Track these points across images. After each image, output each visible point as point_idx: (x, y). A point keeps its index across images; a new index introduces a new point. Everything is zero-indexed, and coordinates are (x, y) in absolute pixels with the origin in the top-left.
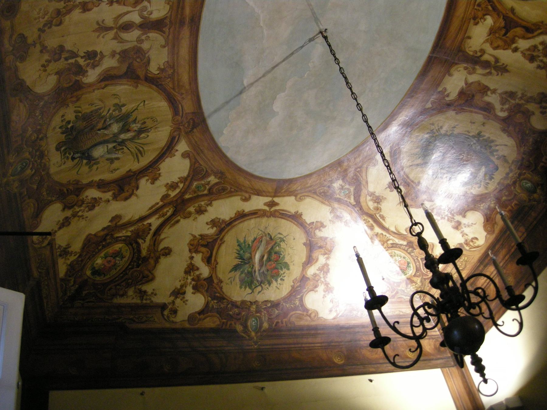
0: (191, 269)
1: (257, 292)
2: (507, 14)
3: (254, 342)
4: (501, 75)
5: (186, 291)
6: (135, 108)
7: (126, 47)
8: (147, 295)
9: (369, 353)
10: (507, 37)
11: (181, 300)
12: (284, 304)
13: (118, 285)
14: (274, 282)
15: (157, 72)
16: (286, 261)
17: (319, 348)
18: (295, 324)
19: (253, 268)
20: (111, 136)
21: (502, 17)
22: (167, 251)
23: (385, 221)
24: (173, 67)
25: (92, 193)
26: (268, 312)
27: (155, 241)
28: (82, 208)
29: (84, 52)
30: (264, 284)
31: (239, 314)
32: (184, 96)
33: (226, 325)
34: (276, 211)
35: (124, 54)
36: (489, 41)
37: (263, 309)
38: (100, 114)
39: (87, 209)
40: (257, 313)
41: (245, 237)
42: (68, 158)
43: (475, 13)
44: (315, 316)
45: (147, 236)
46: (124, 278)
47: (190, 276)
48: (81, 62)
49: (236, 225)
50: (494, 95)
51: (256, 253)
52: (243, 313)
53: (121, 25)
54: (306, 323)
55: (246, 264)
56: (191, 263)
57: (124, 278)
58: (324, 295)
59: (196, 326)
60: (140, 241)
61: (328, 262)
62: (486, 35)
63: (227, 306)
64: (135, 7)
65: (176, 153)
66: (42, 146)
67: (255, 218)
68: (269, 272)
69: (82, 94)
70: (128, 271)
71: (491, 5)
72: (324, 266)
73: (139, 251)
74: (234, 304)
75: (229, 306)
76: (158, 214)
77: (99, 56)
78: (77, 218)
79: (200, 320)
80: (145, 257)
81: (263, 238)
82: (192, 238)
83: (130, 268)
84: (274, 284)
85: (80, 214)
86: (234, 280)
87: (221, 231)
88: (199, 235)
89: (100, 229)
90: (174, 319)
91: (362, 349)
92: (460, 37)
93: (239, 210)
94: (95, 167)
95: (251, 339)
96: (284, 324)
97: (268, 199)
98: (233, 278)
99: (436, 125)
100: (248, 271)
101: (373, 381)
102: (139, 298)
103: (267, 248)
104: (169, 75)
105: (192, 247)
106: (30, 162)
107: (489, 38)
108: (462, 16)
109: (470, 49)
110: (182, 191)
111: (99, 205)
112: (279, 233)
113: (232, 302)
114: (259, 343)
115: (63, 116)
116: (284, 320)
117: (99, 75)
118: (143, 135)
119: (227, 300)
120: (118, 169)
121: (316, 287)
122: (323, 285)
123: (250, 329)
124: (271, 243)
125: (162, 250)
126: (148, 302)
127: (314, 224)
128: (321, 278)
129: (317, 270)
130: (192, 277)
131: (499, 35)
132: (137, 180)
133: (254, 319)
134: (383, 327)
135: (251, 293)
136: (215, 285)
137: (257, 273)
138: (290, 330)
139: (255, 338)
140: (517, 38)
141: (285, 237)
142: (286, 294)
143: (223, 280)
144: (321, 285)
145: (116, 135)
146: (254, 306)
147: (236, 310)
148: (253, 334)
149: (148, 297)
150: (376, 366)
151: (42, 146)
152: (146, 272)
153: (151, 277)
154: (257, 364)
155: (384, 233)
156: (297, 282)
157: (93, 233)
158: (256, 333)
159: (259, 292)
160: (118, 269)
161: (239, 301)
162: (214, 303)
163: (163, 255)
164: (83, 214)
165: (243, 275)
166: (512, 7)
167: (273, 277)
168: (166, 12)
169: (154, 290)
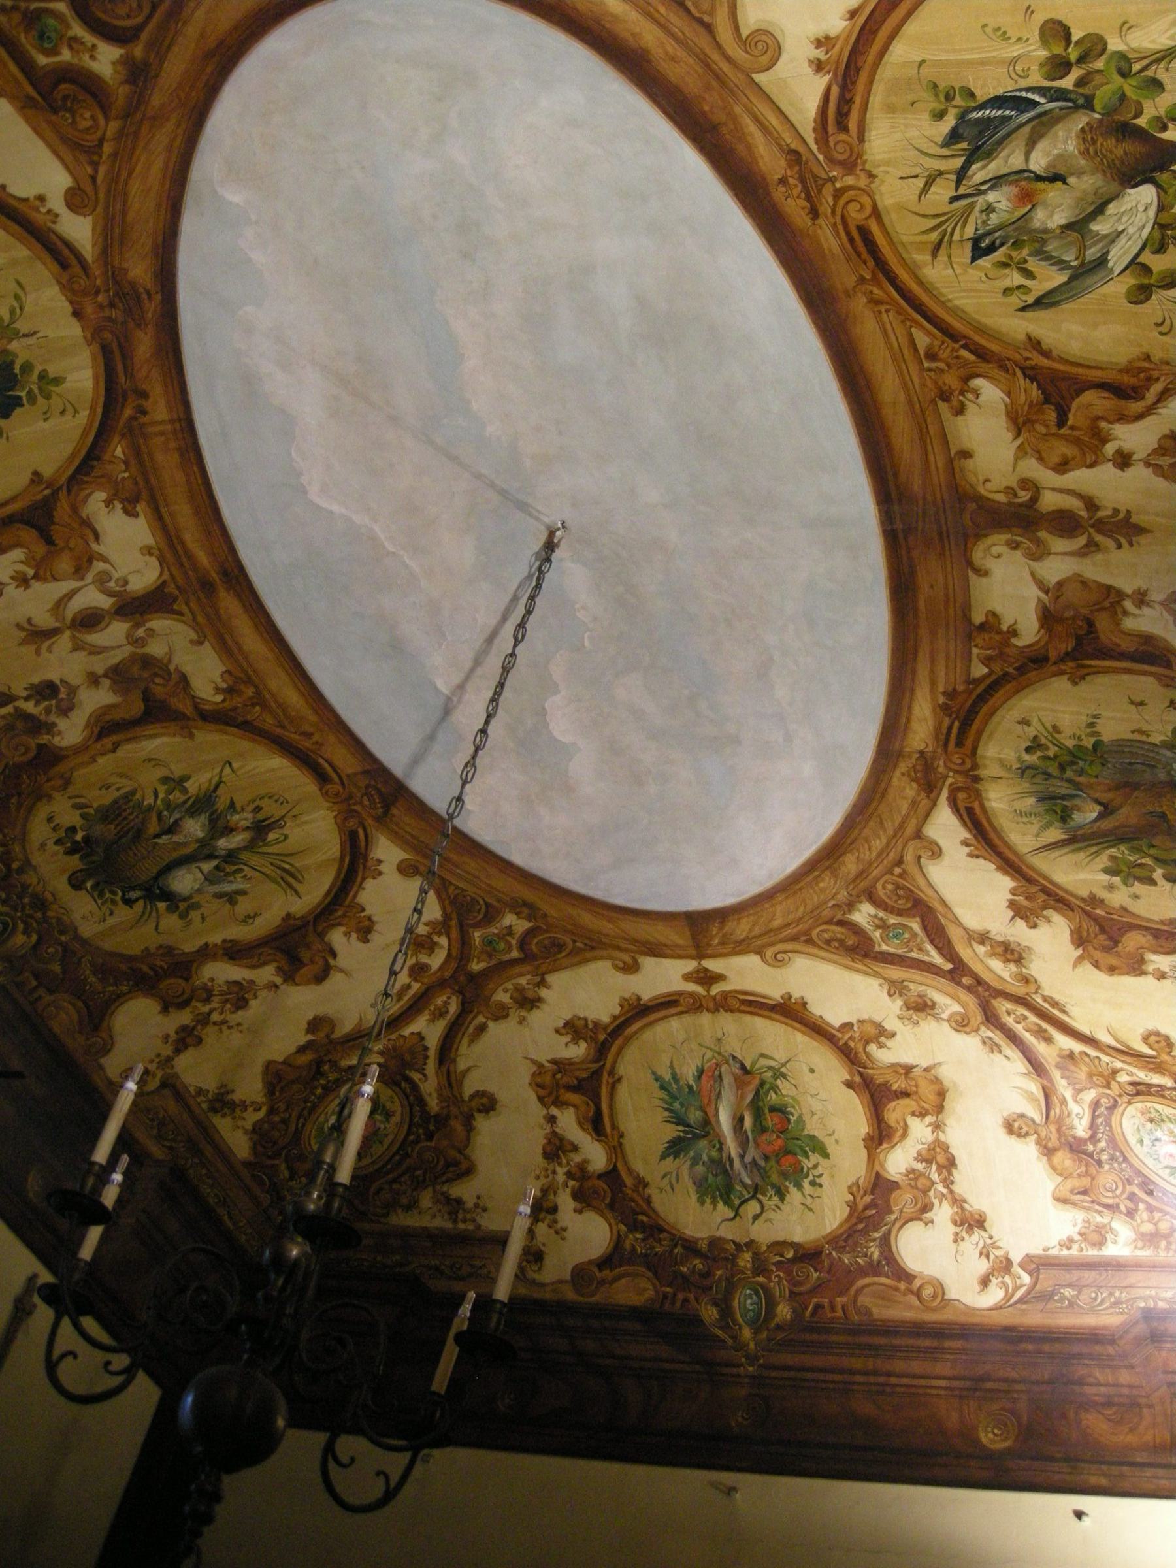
0: (556, 1148)
1: (750, 1216)
2: (1027, 359)
3: (747, 1358)
4: (1131, 545)
5: (559, 1204)
6: (217, 779)
7: (116, 661)
8: (465, 1210)
9: (1105, 1427)
10: (1072, 428)
11: (550, 1227)
12: (834, 1254)
13: (394, 1181)
14: (793, 1190)
15: (219, 698)
16: (812, 1133)
17: (943, 1392)
18: (871, 1314)
19: (720, 1150)
20: (194, 846)
21: (1019, 372)
22: (485, 1100)
23: (469, 1045)
24: (249, 681)
25: (221, 972)
26: (789, 1273)
27: (451, 1081)
28: (214, 1005)
29: (26, 689)
30: (764, 1194)
31: (707, 1274)
32: (316, 738)
33: (673, 1303)
34: (726, 995)
35: (118, 675)
36: (1029, 450)
37: (774, 1264)
38: (139, 804)
39: (228, 1006)
40: (758, 1275)
41: (672, 1067)
42: (113, 902)
43: (936, 383)
44: (934, 1297)
45: (425, 1064)
46: (404, 1167)
47: (560, 1164)
48: (30, 707)
49: (636, 1033)
50: (1146, 610)
51: (717, 1110)
52: (719, 1273)
53: (74, 620)
54: (909, 1315)
55: (697, 1137)
56: (554, 1133)
57: (404, 1167)
58: (957, 1234)
59: (593, 1299)
60: (416, 1076)
61: (942, 1137)
62: (1010, 436)
63: (671, 1251)
64: (82, 579)
65: (382, 868)
66: (30, 885)
67: (677, 1014)
68: (773, 1163)
69: (72, 770)
70: (410, 1149)
71: (965, 347)
72: (934, 1149)
73: (421, 1102)
74: (690, 1247)
75: (678, 1250)
76: (427, 1012)
77: (62, 689)
78: (210, 1030)
79: (602, 1282)
80: (437, 1116)
81: (723, 1069)
82: (534, 1068)
83: (412, 1142)
84: (794, 1195)
85: (215, 1017)
86: (678, 1180)
87: (602, 1050)
88: (549, 1061)
89: (293, 1049)
90: (536, 1276)
91: (1087, 1410)
92: (938, 460)
93: (627, 996)
94: (195, 915)
95: (740, 1346)
96: (839, 1313)
97: (690, 965)
98: (674, 1175)
99: (1035, 721)
100: (709, 1156)
101: (1084, 1518)
102: (446, 1216)
103: (742, 1098)
104: (251, 698)
105: (542, 1092)
106: (12, 918)
107: (1022, 443)
108: (902, 397)
109: (989, 485)
110: (454, 954)
111: (256, 997)
112: (763, 1055)
113: (681, 1239)
114: (761, 1361)
115: (50, 820)
116: (838, 1299)
117: (86, 727)
118: (271, 836)
119: (668, 1232)
120: (256, 915)
121: (927, 1208)
122: (945, 1204)
123: (738, 1316)
124: (750, 1082)
125: (473, 1097)
126: (471, 1227)
127: (855, 1028)
128: (933, 1183)
129: (915, 1159)
130: (565, 1170)
131: (1047, 426)
132: (321, 935)
133: (748, 1292)
134: (1169, 1345)
135: (734, 1218)
136: (630, 1192)
137: (737, 1163)
138: (855, 1331)
139: (752, 1345)
140: (1103, 424)
141: (784, 1065)
142: (835, 1226)
143: (648, 1178)
144: (941, 1203)
145: (203, 843)
146: (748, 1256)
147: (697, 1261)
148: (747, 1333)
149: (468, 1216)
150: (1115, 1470)
151: (30, 885)
152: (453, 1153)
153: (464, 1166)
154: (740, 1419)
155: (1093, 1053)
156: (862, 1192)
157: (281, 1059)
158: (757, 1332)
159: (756, 1217)
160: (387, 1142)
161: (703, 1239)
162: (634, 1240)
163: (480, 1111)
164: (223, 1016)
165: (700, 1168)
166: (1029, 337)
167: (785, 1175)
168: (157, 573)
169: (478, 1197)
